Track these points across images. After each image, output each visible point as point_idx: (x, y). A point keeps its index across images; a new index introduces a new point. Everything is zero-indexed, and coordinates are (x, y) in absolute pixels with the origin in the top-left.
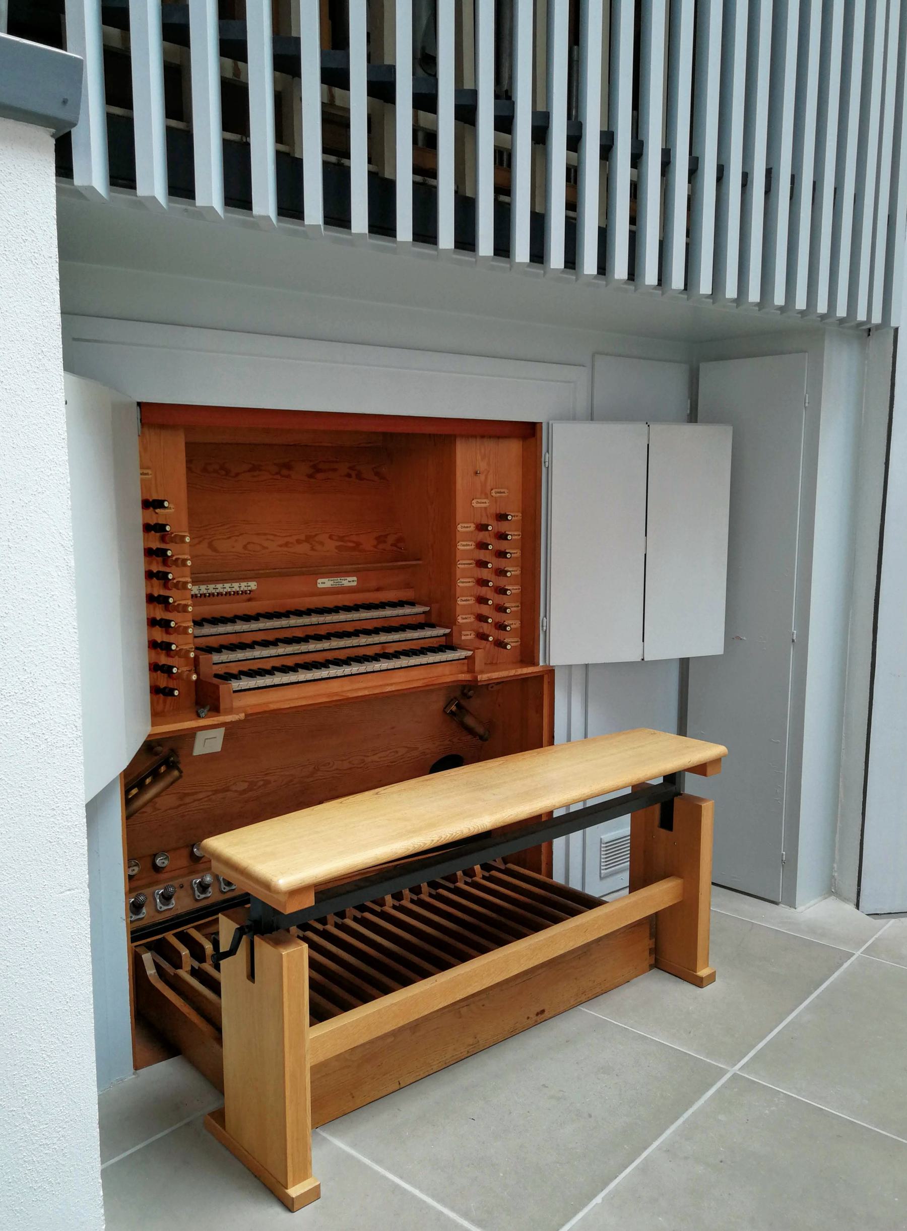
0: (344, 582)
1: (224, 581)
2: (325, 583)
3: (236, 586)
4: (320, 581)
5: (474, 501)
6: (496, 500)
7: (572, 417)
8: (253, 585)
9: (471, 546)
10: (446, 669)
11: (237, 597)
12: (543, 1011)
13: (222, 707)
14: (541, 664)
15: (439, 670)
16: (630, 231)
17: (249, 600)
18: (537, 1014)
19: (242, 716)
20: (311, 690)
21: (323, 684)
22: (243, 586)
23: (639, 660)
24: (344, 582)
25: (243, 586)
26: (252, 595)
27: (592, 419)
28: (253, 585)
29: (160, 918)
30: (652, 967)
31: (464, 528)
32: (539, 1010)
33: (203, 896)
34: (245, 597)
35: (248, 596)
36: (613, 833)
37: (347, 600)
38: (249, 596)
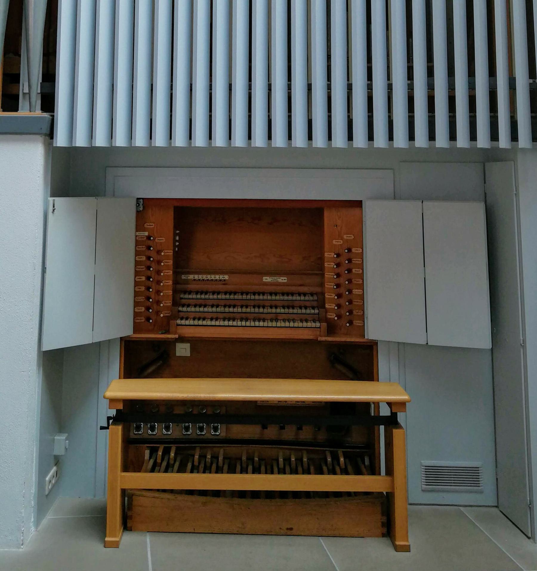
0: (278, 280)
2: (267, 279)
4: (264, 278)
7: (380, 197)
8: (226, 277)
9: (333, 265)
10: (306, 331)
12: (291, 529)
13: (171, 331)
14: (366, 338)
15: (300, 331)
17: (224, 284)
19: (177, 336)
20: (212, 330)
21: (228, 329)
22: (221, 277)
23: (425, 343)
24: (278, 280)
26: (226, 282)
27: (395, 199)
28: (226, 277)
30: (383, 535)
31: (329, 255)
34: (222, 282)
35: (224, 282)
36: (430, 461)
37: (278, 289)
38: (224, 282)
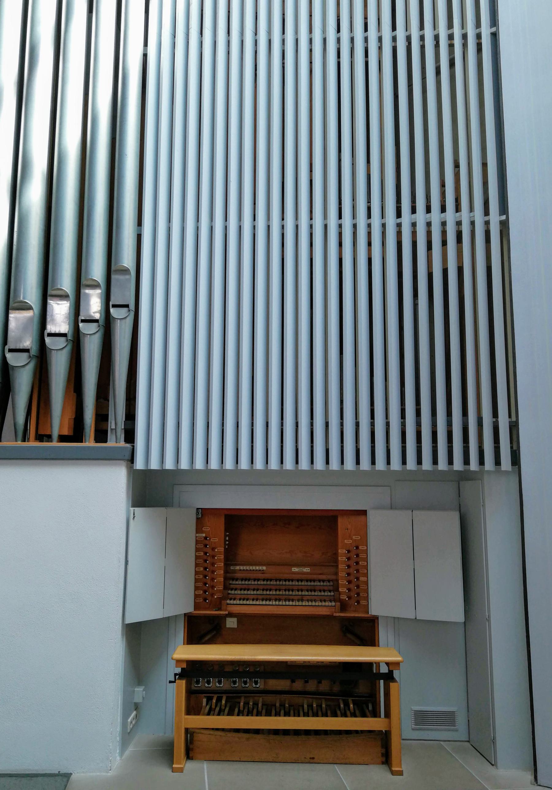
1: (252, 565)
2: (295, 569)
3: (257, 568)
5: (360, 538)
6: (355, 540)
8: (264, 568)
11: (240, 572)
12: (313, 758)
16: (406, 443)
18: (310, 758)
22: (260, 568)
23: (414, 618)
25: (260, 568)
27: (391, 509)
28: (264, 568)
29: (203, 688)
32: (312, 757)
33: (218, 685)
37: (304, 577)
38: (263, 572)
